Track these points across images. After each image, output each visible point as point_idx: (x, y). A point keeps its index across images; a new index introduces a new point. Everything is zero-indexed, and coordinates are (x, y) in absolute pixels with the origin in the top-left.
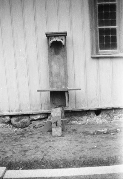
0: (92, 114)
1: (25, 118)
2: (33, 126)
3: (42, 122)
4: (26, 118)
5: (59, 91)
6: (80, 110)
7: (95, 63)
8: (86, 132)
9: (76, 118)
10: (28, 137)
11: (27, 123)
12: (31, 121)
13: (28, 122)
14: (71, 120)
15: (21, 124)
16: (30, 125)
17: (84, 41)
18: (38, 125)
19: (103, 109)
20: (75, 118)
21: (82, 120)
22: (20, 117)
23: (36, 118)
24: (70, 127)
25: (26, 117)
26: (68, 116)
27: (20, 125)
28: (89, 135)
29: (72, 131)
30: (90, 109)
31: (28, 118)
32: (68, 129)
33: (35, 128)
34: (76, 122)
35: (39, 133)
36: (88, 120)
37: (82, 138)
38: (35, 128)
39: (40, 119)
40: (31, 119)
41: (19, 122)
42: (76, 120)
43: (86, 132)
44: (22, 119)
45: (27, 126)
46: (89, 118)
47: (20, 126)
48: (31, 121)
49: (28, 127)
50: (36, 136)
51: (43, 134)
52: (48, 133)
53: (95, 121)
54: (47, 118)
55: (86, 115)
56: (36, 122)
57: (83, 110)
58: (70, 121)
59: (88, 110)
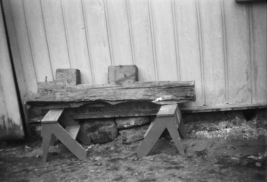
0: (237, 118)
1: (106, 123)
2: (123, 140)
3: (138, 133)
4: (109, 125)
5: (21, 114)
6: (213, 109)
7: (245, 14)
8: (225, 158)
9: (205, 125)
10: (109, 167)
11: (110, 133)
12: (119, 129)
13: (114, 131)
14: (197, 129)
15: (100, 136)
16: (116, 137)
17: (227, 59)
18: (132, 138)
19: (260, 108)
20: (203, 124)
21: (218, 130)
22: (97, 123)
23: (127, 124)
24: (193, 145)
25: (109, 122)
26: (190, 121)
27: (98, 138)
28: (230, 168)
29: (196, 156)
30: (233, 108)
31: (112, 125)
32: (189, 149)
33: (127, 144)
34: (206, 133)
35: (132, 158)
36: (228, 130)
37: (213, 175)
38: (127, 144)
39: (136, 127)
40: (118, 125)
41: (96, 133)
42: (205, 129)
43: (225, 158)
44: (102, 125)
45: (111, 140)
46: (231, 125)
47: (98, 140)
48: (119, 129)
49: (113, 143)
50: (124, 164)
51: (138, 160)
52: (149, 157)
53: (244, 132)
54: (149, 124)
55: (226, 120)
56: (128, 132)
57: (219, 109)
58: (194, 131)
59: (229, 110)
